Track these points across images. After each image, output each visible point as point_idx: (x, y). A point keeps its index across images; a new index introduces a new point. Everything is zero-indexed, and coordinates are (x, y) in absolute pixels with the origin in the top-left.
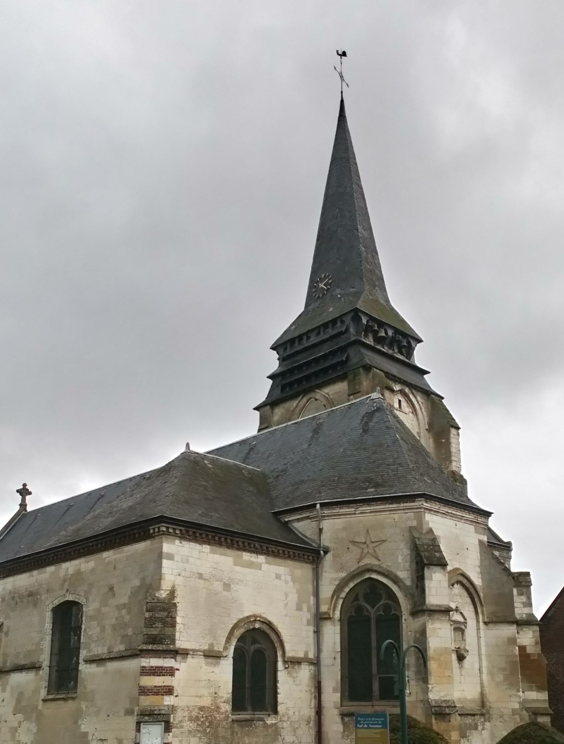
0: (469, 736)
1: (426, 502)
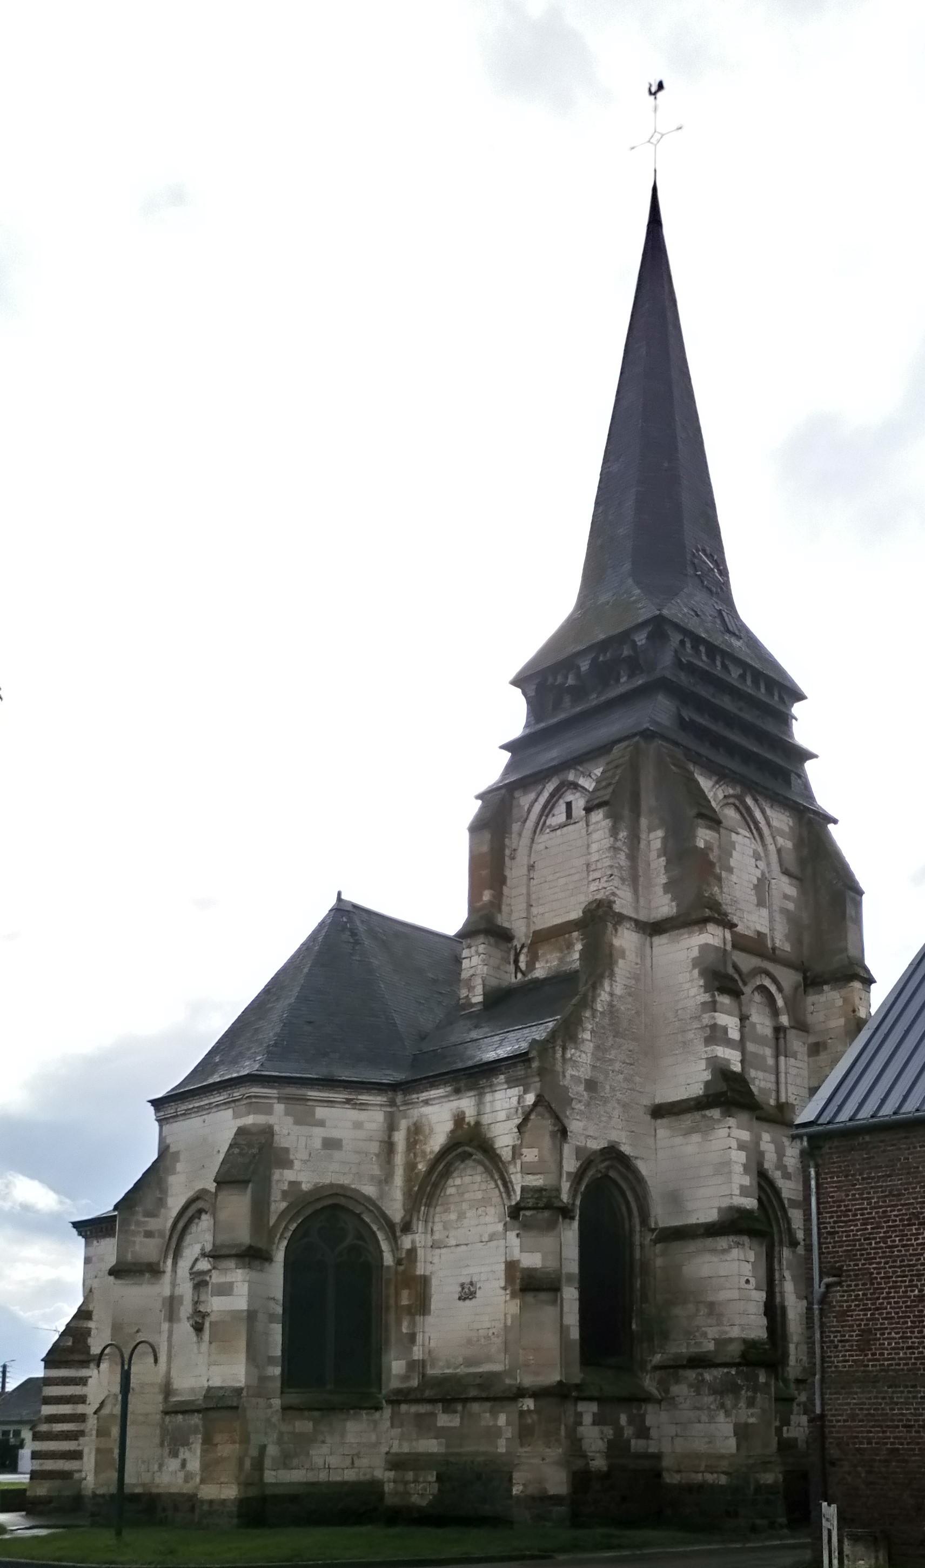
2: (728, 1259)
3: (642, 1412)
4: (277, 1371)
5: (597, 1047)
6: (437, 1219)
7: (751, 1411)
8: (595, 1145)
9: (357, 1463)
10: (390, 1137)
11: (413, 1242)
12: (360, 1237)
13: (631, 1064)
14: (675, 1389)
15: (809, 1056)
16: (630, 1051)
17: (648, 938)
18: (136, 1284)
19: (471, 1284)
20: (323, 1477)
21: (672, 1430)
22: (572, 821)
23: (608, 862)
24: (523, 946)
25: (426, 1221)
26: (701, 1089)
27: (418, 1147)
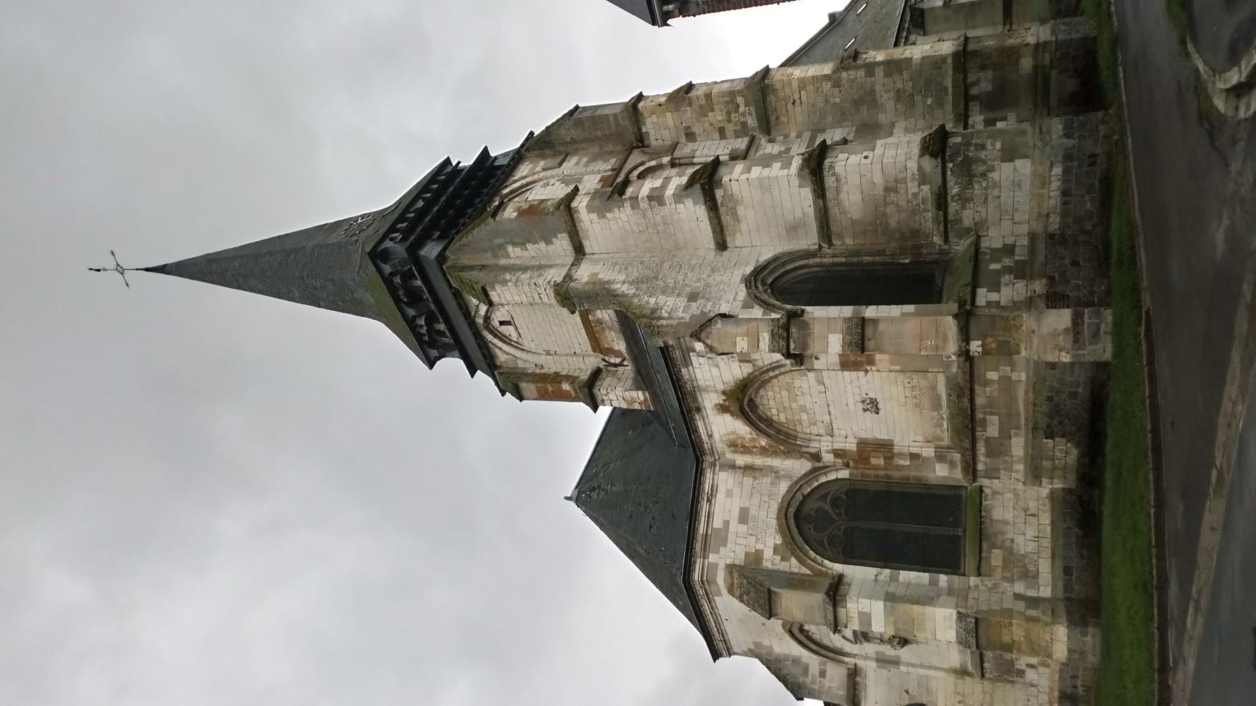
2: (844, 175)
3: (988, 251)
4: (943, 579)
5: (663, 293)
6: (808, 431)
7: (989, 147)
8: (742, 293)
9: (1033, 511)
10: (740, 468)
11: (828, 452)
12: (824, 497)
13: (681, 266)
14: (967, 222)
15: (696, 141)
16: (670, 268)
17: (586, 256)
18: (865, 689)
19: (863, 402)
20: (1047, 543)
21: (1006, 224)
22: (512, 320)
23: (526, 288)
24: (604, 360)
25: (810, 441)
26: (700, 208)
27: (747, 445)
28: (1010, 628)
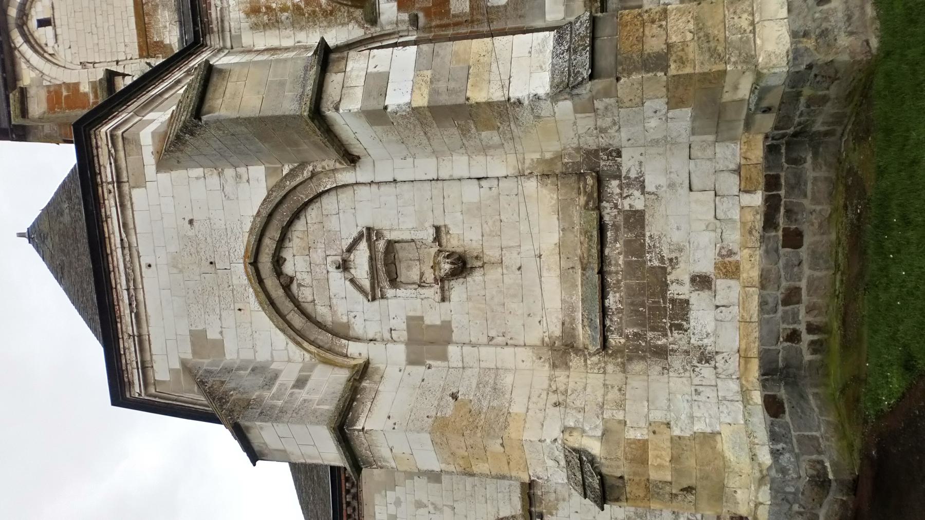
0: (662, 260)
1: (131, 384)
28: (664, 23)
